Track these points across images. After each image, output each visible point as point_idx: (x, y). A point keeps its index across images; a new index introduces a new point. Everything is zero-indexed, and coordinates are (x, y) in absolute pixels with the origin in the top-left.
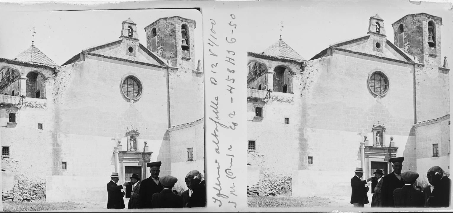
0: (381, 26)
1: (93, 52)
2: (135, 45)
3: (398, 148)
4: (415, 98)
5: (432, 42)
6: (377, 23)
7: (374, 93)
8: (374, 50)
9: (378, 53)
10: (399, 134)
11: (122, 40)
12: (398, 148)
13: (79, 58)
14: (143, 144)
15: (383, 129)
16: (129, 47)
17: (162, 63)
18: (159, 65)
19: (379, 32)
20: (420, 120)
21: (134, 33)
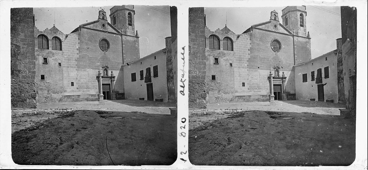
0: (105, 15)
1: (86, 27)
2: (106, 23)
3: (286, 77)
4: (294, 53)
5: (302, 24)
6: (102, 14)
7: (274, 50)
8: (273, 29)
9: (275, 30)
10: (115, 70)
11: (271, 21)
12: (286, 77)
13: (78, 30)
14: (111, 72)
15: (108, 67)
16: (103, 24)
17: (119, 32)
18: (289, 34)
19: (104, 18)
20: (297, 63)
21: (277, 18)
